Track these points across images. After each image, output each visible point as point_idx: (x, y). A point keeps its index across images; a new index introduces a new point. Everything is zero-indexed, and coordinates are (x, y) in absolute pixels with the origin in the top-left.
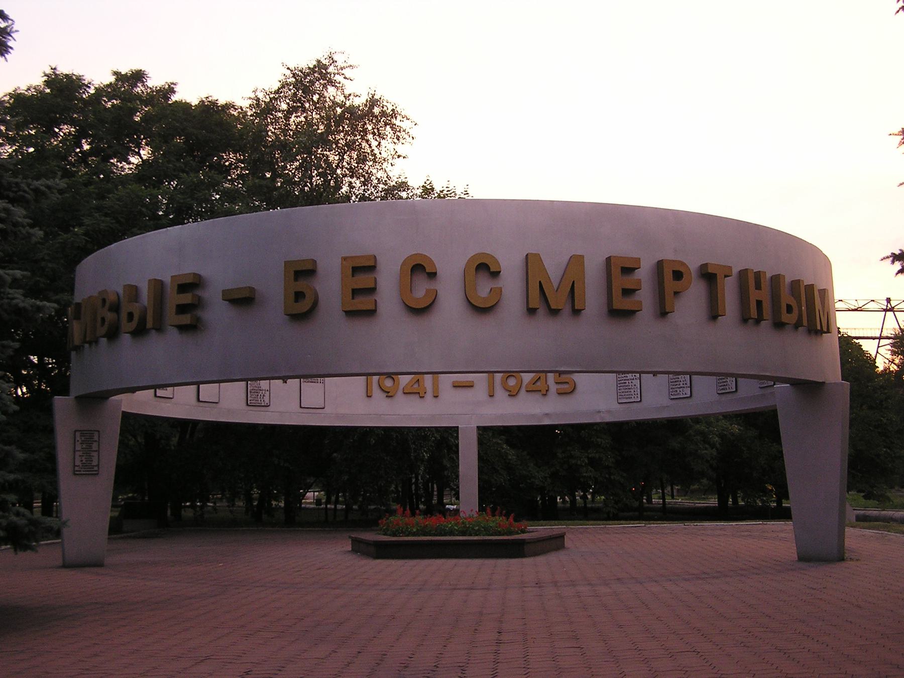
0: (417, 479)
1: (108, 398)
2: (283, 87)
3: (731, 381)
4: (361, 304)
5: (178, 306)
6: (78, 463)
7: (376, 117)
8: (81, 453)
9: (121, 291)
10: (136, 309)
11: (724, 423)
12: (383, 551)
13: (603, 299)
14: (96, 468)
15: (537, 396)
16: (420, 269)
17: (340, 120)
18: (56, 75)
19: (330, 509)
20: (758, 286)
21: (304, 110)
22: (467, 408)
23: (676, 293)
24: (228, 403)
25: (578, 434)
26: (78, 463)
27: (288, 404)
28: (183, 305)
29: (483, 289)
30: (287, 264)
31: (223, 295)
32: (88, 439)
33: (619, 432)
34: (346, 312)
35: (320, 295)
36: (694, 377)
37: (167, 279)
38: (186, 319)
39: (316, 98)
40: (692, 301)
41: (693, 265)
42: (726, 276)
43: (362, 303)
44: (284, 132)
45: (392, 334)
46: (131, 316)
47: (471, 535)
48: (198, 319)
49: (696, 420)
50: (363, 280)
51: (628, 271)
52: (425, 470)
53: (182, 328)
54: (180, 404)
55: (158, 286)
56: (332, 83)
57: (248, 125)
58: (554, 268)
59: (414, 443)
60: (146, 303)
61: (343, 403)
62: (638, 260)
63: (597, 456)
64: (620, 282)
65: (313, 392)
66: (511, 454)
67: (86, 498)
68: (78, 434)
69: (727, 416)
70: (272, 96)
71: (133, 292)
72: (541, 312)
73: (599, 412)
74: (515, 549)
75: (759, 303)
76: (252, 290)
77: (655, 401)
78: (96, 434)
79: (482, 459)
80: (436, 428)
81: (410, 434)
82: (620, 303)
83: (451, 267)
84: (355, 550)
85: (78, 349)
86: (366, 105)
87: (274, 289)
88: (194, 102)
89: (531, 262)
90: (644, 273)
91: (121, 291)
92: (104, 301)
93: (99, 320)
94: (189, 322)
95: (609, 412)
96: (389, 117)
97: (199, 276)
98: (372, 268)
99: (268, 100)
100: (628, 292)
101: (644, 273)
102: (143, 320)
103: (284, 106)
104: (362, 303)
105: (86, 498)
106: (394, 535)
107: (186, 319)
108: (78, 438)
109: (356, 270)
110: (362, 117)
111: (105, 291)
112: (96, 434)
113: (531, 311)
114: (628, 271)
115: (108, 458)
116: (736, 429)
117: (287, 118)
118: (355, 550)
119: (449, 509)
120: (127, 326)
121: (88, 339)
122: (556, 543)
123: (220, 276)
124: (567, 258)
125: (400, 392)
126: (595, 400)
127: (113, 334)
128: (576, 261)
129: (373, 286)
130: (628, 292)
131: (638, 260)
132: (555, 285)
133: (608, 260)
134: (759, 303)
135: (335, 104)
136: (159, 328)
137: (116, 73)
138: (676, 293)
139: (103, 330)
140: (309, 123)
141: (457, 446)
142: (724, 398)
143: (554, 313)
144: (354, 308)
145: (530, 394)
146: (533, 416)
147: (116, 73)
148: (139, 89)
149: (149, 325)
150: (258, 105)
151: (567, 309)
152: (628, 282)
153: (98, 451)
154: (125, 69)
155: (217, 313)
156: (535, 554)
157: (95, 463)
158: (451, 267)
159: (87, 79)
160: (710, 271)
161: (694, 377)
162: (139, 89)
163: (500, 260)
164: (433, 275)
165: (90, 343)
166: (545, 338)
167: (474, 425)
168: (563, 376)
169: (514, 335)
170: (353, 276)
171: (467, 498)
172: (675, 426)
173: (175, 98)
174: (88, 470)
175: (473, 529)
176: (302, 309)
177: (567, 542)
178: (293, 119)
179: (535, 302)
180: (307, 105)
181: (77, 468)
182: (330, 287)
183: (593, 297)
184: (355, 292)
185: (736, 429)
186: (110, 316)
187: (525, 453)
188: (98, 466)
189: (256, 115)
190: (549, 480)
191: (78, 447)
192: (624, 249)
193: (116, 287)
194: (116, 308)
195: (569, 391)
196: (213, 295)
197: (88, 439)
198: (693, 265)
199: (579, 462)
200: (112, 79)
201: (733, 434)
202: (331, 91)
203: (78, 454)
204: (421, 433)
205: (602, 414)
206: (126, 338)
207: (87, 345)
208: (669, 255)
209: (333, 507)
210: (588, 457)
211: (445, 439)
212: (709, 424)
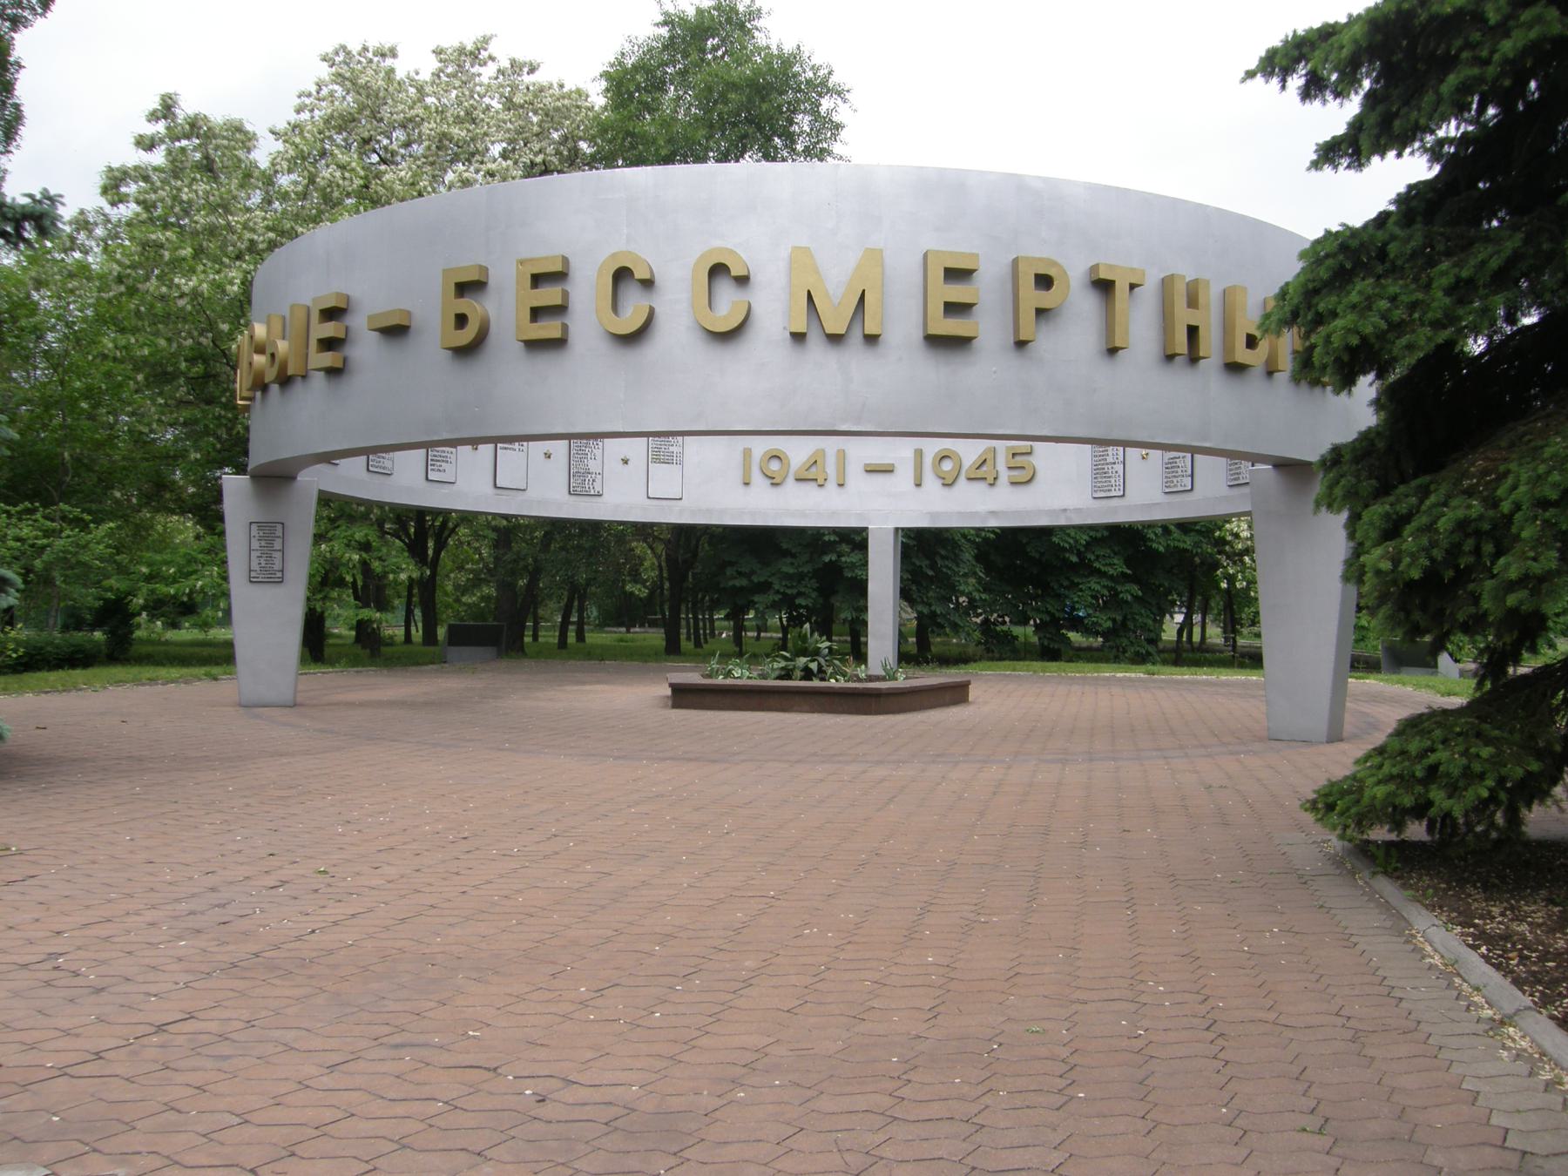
5: (321, 341)
6: (255, 566)
13: (916, 317)
15: (981, 486)
20: (1192, 302)
22: (882, 498)
23: (1041, 312)
26: (255, 566)
36: (1197, 456)
38: (328, 359)
41: (1074, 270)
43: (548, 329)
50: (548, 295)
65: (665, 480)
67: (265, 619)
68: (254, 527)
72: (815, 339)
75: (1193, 331)
89: (801, 260)
95: (1078, 511)
98: (559, 276)
104: (548, 329)
105: (265, 619)
109: (537, 280)
112: (279, 527)
113: (1170, 358)
125: (790, 480)
126: (1060, 492)
128: (873, 257)
129: (559, 302)
134: (1193, 331)
142: (1236, 491)
146: (974, 514)
147: (438, 52)
155: (366, 348)
159: (1352, 172)
161: (1197, 456)
167: (892, 526)
168: (1018, 458)
174: (274, 578)
182: (504, 308)
183: (902, 321)
184: (536, 313)
196: (358, 322)
197: (270, 532)
198: (1074, 270)
211: (856, 539)
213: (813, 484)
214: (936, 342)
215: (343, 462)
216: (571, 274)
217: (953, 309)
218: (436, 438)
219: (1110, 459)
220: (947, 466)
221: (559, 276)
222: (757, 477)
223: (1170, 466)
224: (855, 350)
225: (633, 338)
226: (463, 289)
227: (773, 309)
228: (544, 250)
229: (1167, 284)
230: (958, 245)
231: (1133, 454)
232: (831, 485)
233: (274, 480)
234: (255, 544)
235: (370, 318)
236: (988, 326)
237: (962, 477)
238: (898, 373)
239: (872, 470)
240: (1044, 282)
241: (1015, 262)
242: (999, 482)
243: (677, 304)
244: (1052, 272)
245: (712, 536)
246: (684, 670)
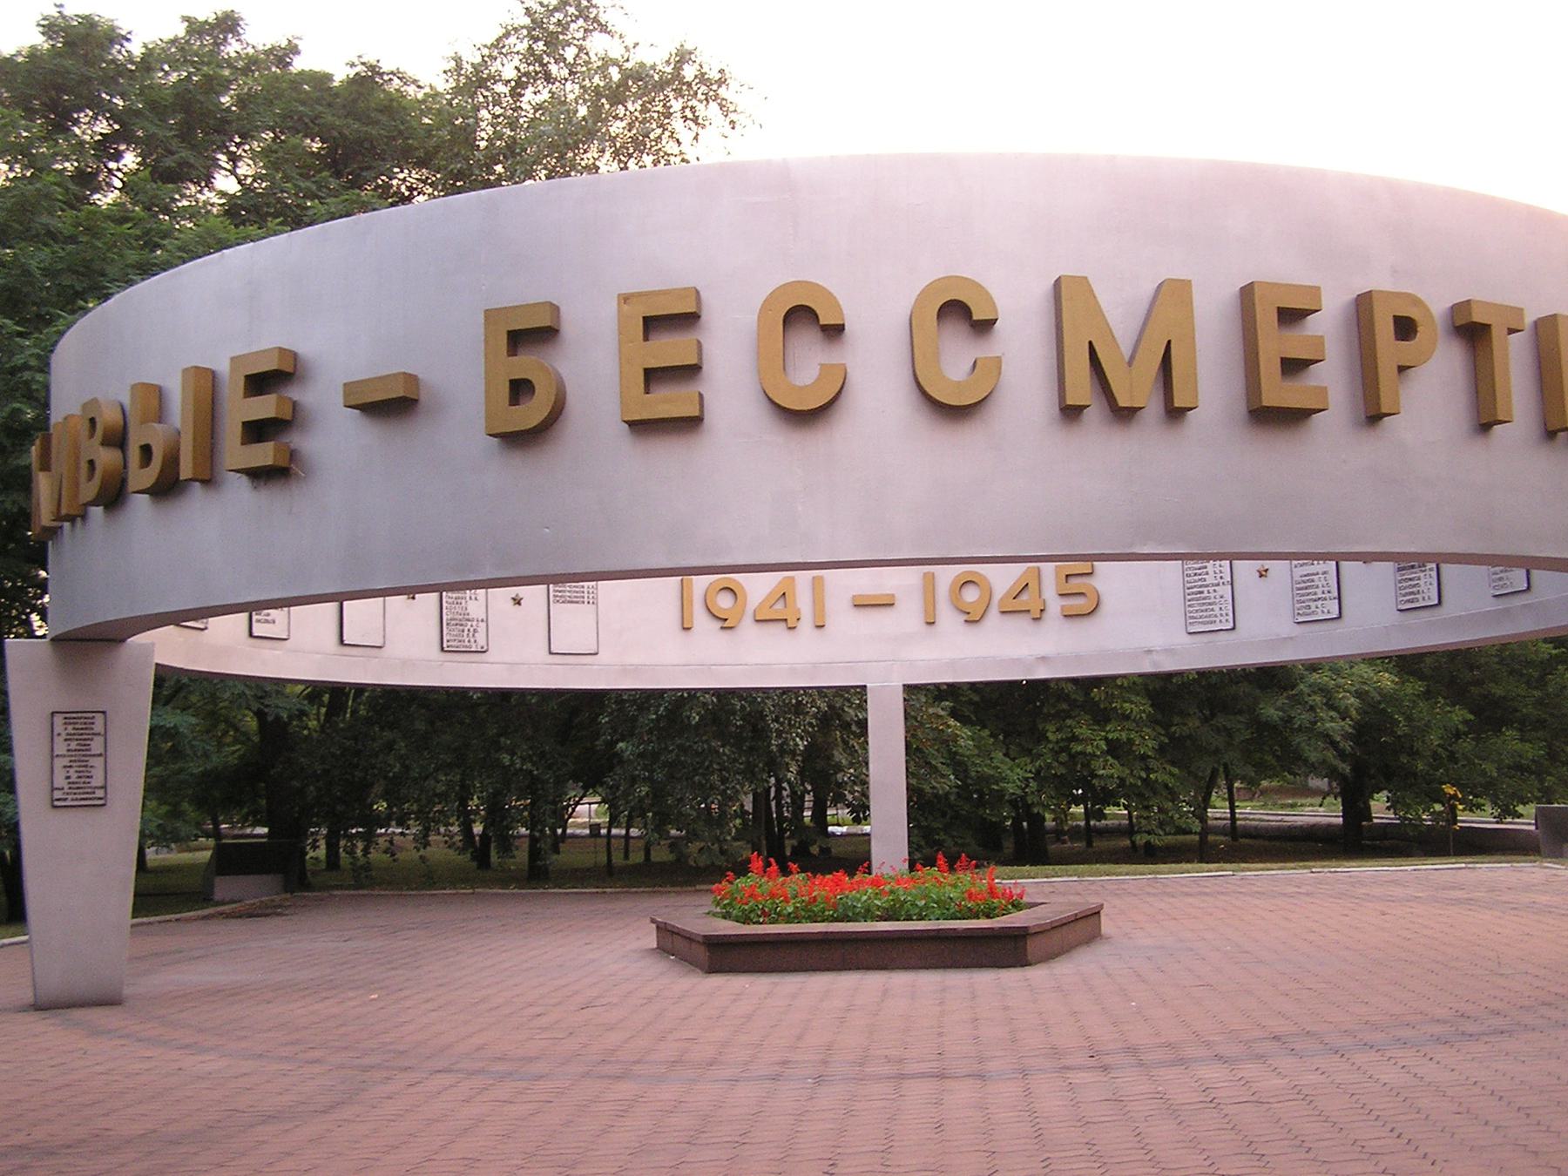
0: (779, 789)
1: (123, 641)
2: (507, 35)
3: (1517, 578)
4: (666, 404)
6: (60, 781)
7: (689, 85)
8: (66, 761)
9: (126, 400)
10: (157, 437)
11: (1365, 670)
12: (724, 956)
14: (100, 793)
15: (1022, 622)
16: (803, 317)
17: (617, 95)
18: (64, 17)
19: (616, 837)
21: (548, 78)
22: (883, 645)
23: (1402, 369)
24: (401, 645)
25: (1085, 697)
26: (60, 781)
27: (523, 645)
28: (261, 423)
29: (956, 362)
30: (489, 314)
31: (346, 395)
32: (81, 728)
33: (1167, 692)
34: (632, 424)
35: (568, 390)
37: (222, 366)
38: (264, 454)
39: (570, 53)
40: (1434, 384)
42: (1511, 331)
43: (669, 401)
44: (513, 125)
45: (740, 473)
46: (146, 451)
47: (909, 918)
48: (293, 455)
49: (1313, 666)
50: (669, 349)
51: (1291, 316)
52: (800, 773)
53: (260, 475)
54: (302, 649)
55: (205, 384)
56: (604, 28)
57: (445, 116)
58: (1120, 310)
59: (776, 720)
60: (178, 424)
61: (630, 640)
62: (1315, 292)
63: (1124, 736)
64: (1275, 343)
65: (574, 622)
66: (965, 737)
67: (82, 858)
68: (59, 719)
69: (1371, 660)
70: (486, 52)
71: (153, 399)
72: (1095, 413)
73: (1149, 652)
74: (1008, 949)
76: (411, 379)
77: (1262, 624)
78: (99, 718)
79: (913, 750)
80: (819, 689)
81: (769, 702)
82: (1278, 392)
83: (878, 314)
84: (663, 949)
85: (53, 532)
86: (668, 63)
87: (462, 377)
88: (340, 74)
90: (1327, 325)
91: (126, 400)
92: (92, 421)
93: (84, 466)
94: (270, 462)
95: (1169, 651)
96: (712, 86)
97: (295, 355)
98: (688, 320)
99: (478, 60)
100: (1293, 367)
101: (1327, 325)
102: (172, 460)
103: (509, 73)
104: (669, 401)
105: (82, 858)
106: (746, 920)
107: (264, 454)
108: (58, 728)
109: (652, 324)
110: (662, 85)
111: (95, 401)
112: (1230, 626)
113: (1071, 413)
114: (1291, 316)
115: (127, 767)
116: (1387, 680)
117: (516, 94)
118: (663, 949)
119: (833, 834)
120: (142, 477)
121: (64, 512)
122: (1082, 928)
123: (340, 354)
124: (1148, 288)
125: (748, 620)
126: (1141, 626)
127: (113, 496)
128: (1172, 295)
129: (693, 361)
130: (1293, 367)
131: (1315, 292)
132: (1126, 350)
133: (1247, 294)
135: (607, 62)
136: (209, 481)
137: (186, 19)
138: (1402, 369)
139: (89, 490)
140: (557, 101)
141: (863, 724)
143: (1124, 415)
144: (645, 416)
145: (1006, 617)
148: (232, 48)
149: (186, 472)
150: (459, 67)
151: (1153, 407)
152: (1293, 343)
153: (104, 755)
154: (205, 14)
155: (334, 438)
156: (1049, 957)
157: (97, 781)
158: (878, 314)
159: (124, 26)
160: (1475, 319)
161: (1343, 564)
162: (232, 48)
163: (994, 292)
164: (834, 332)
165: (72, 519)
166: (1102, 474)
168: (1073, 581)
169: (1026, 468)
170: (646, 338)
171: (888, 829)
172: (1271, 678)
173: (299, 64)
174: (82, 796)
175: (914, 905)
176: (529, 421)
177: (1106, 926)
178: (528, 94)
179: (1081, 388)
180: (554, 69)
181: (58, 794)
182: (594, 367)
183: (1213, 380)
184: (653, 376)
185: (1387, 680)
186: (107, 458)
187: (986, 733)
188: (104, 787)
189: (457, 91)
190: (1033, 784)
191: (61, 747)
192: (1283, 267)
193: (114, 393)
194: (117, 439)
195: (1085, 609)
196: (322, 397)
197: (81, 728)
198: (1438, 302)
199: (1089, 749)
200: (180, 30)
201: (1379, 690)
202: (598, 44)
203: (59, 763)
204: (791, 701)
205: (1155, 657)
206: (141, 504)
207: (67, 525)
208: (1380, 282)
209: (623, 832)
210: (1106, 739)
211: (836, 714)
212: (1336, 671)
213: (783, 624)
215: (214, 622)
216: (704, 317)
218: (472, 577)
219: (1210, 580)
220: (971, 595)
221: (688, 320)
222: (700, 618)
223: (1302, 588)
226: (520, 339)
228: (664, 269)
229: (1363, 305)
231: (1246, 569)
232: (806, 625)
233: (90, 644)
234: (61, 747)
235: (349, 388)
237: (994, 611)
239: (861, 605)
242: (800, 625)
245: (474, 706)
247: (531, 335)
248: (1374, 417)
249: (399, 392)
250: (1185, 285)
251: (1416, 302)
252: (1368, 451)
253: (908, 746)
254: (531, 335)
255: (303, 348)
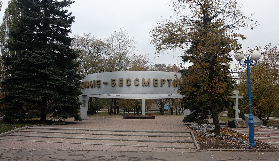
4: (121, 85)
10: (92, 84)
23: (163, 83)
28: (98, 84)
30: (112, 79)
38: (98, 86)
41: (166, 80)
48: (100, 86)
50: (121, 82)
55: (95, 81)
58: (146, 80)
72: (145, 86)
87: (110, 82)
95: (166, 97)
102: (93, 86)
107: (98, 86)
113: (143, 86)
128: (149, 79)
136: (95, 87)
138: (163, 83)
143: (146, 86)
149: (93, 86)
154: (86, 33)
155: (102, 85)
176: (114, 85)
182: (117, 82)
183: (152, 84)
196: (102, 83)
214: (154, 86)
217: (156, 83)
224: (148, 87)
225: (129, 86)
226: (113, 81)
227: (141, 83)
228: (121, 77)
230: (156, 78)
233: (85, 96)
236: (159, 84)
238: (151, 88)
240: (164, 81)
241: (161, 79)
243: (133, 83)
244: (164, 80)
246: (49, 127)
247: (114, 80)
248: (162, 86)
249: (106, 83)
250: (150, 79)
251: (164, 79)
252: (161, 88)
253: (119, 99)
254: (114, 80)
255: (101, 80)
